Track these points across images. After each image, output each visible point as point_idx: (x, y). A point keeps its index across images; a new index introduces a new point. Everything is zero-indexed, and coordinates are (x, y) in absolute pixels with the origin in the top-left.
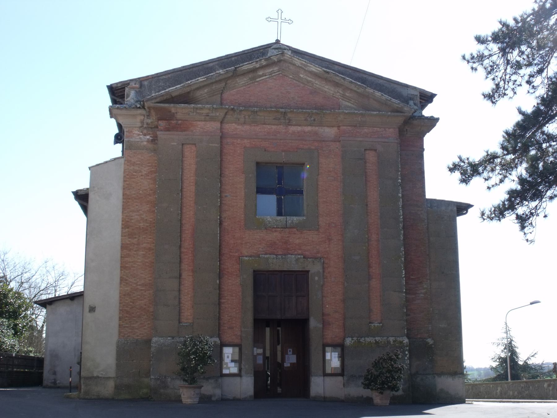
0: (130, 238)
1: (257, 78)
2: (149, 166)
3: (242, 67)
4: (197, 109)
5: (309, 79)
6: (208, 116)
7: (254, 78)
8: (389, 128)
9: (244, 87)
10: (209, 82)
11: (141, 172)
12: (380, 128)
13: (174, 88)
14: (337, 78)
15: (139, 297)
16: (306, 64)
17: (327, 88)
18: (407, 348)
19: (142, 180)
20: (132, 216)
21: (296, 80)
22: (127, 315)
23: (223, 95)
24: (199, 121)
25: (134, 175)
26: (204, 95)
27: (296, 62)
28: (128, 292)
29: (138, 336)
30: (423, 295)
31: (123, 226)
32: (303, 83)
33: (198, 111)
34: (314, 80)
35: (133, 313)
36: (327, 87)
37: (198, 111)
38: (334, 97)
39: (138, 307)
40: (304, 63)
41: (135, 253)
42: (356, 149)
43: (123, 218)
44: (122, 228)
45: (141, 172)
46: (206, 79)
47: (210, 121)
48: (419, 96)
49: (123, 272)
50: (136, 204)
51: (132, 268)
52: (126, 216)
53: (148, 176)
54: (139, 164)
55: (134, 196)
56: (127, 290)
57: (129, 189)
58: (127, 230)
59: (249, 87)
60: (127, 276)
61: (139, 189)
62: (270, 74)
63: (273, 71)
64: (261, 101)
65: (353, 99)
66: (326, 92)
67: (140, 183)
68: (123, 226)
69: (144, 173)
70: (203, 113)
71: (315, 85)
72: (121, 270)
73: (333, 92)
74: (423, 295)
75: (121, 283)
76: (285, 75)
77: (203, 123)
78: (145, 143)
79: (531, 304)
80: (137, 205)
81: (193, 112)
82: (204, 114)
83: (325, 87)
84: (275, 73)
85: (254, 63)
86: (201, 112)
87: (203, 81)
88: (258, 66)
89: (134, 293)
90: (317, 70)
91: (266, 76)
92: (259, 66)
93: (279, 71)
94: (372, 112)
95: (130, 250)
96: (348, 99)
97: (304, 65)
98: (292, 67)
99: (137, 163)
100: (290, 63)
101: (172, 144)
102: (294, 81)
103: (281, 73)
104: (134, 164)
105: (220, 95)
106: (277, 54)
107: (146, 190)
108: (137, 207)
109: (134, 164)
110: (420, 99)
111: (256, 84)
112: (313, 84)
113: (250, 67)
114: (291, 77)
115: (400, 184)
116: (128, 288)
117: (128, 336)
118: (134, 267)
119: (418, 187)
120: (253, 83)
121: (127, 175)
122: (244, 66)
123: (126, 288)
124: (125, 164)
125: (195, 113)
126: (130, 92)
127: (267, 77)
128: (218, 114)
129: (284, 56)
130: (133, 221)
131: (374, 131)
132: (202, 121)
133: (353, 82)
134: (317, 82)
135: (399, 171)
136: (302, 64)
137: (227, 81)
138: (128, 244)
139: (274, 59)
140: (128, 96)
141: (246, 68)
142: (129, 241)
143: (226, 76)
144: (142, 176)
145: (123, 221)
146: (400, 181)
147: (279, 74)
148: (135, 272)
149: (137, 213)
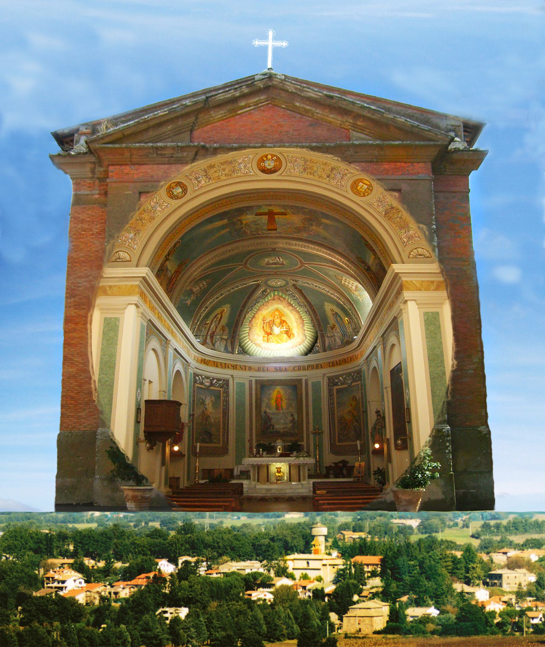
0: (75, 309)
1: (239, 111)
2: (102, 223)
3: (216, 97)
4: (157, 148)
5: (308, 108)
6: (172, 157)
7: (234, 110)
8: (418, 163)
9: (222, 122)
10: (172, 116)
11: (91, 230)
12: (405, 163)
13: (126, 124)
14: (344, 103)
15: (87, 379)
16: (302, 88)
17: (332, 118)
18: (449, 438)
19: (92, 240)
20: (79, 283)
21: (291, 111)
22: (72, 402)
23: (194, 133)
24: (162, 164)
25: (83, 234)
26: (167, 133)
27: (288, 87)
28: (73, 374)
29: (85, 427)
30: (472, 372)
31: (68, 295)
32: (300, 114)
33: (159, 152)
34: (314, 109)
35: (80, 400)
36: (332, 116)
37: (159, 152)
38: (343, 128)
39: (85, 392)
40: (299, 87)
41: (83, 326)
42: (314, 144)
43: (67, 286)
44: (67, 297)
45: (91, 230)
46: (167, 112)
47: (175, 164)
48: (462, 126)
49: (67, 350)
50: (85, 268)
51: (79, 345)
52: (72, 283)
53: (101, 234)
54: (89, 221)
55: (82, 259)
56: (72, 372)
57: (76, 251)
58: (72, 300)
59: (228, 122)
60: (72, 355)
61: (88, 251)
62: (256, 105)
63: (259, 100)
64: (243, 137)
65: (367, 129)
66: (330, 122)
67: (90, 244)
68: (68, 295)
69: (95, 231)
70: (165, 154)
71: (315, 114)
72: (64, 348)
73: (340, 122)
74: (472, 372)
75: (64, 364)
76: (275, 105)
77: (167, 166)
78: (97, 196)
79: (370, 609)
80: (86, 270)
81: (153, 154)
82: (167, 156)
83: (329, 116)
84: (262, 103)
85: (232, 91)
86: (163, 152)
87: (164, 115)
88: (237, 94)
89: (81, 375)
90: (316, 95)
91: (250, 107)
92: (238, 94)
93: (268, 101)
94: (392, 143)
95: (76, 324)
96: (361, 130)
97: (300, 90)
98: (283, 94)
99: (87, 219)
100: (281, 89)
101: (126, 193)
102: (289, 112)
103: (271, 103)
104: (83, 221)
105: (189, 133)
106: (263, 79)
107: (97, 251)
108: (86, 272)
109: (83, 221)
110: (464, 131)
111: (237, 117)
112: (313, 114)
113: (228, 96)
114: (284, 106)
115: (435, 231)
116: (73, 370)
117: (72, 428)
118: (81, 344)
119: (462, 236)
120: (233, 116)
121: (74, 234)
122: (218, 95)
123: (71, 370)
124: (71, 221)
125: (155, 155)
126: (79, 139)
127: (251, 108)
128: (185, 154)
129: (273, 80)
130: (80, 289)
131: (398, 167)
132: (165, 164)
133: (366, 107)
134: (317, 111)
135: (432, 215)
136: (296, 89)
137: (198, 115)
138: (74, 316)
139: (259, 85)
140: (78, 142)
141: (222, 98)
142: (75, 313)
143: (194, 108)
144: (92, 235)
145: (67, 289)
146: (434, 227)
147: (268, 104)
148: (82, 350)
149: (86, 279)
